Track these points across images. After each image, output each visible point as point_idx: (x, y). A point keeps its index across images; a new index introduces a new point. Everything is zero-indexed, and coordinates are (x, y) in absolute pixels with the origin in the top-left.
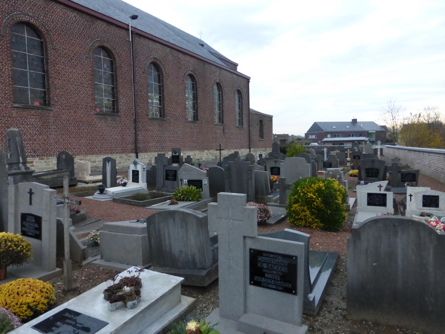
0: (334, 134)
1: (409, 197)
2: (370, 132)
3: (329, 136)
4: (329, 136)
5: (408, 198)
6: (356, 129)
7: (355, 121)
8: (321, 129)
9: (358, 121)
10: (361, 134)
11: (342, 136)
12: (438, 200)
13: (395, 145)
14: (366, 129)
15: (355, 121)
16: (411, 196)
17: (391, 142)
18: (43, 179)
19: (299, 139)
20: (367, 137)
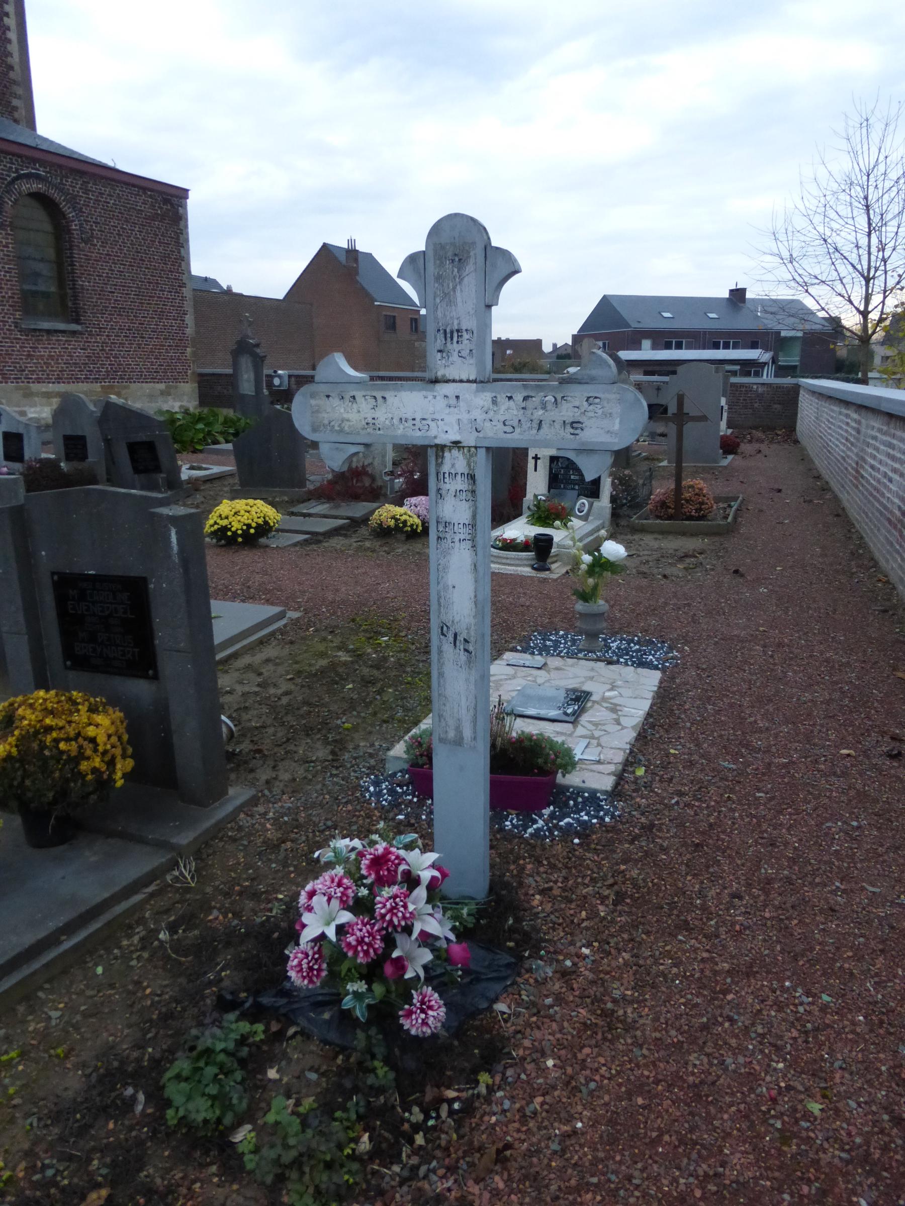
0: (665, 338)
1: (533, 461)
2: (783, 334)
3: (647, 343)
4: (647, 343)
5: (531, 463)
6: (742, 323)
7: (738, 295)
8: (621, 321)
9: (749, 295)
10: (753, 340)
11: (689, 347)
12: (85, 446)
13: (864, 381)
14: (771, 323)
15: (738, 295)
16: (536, 458)
17: (850, 372)
18: (272, 504)
19: (190, 272)
20: (766, 349)
